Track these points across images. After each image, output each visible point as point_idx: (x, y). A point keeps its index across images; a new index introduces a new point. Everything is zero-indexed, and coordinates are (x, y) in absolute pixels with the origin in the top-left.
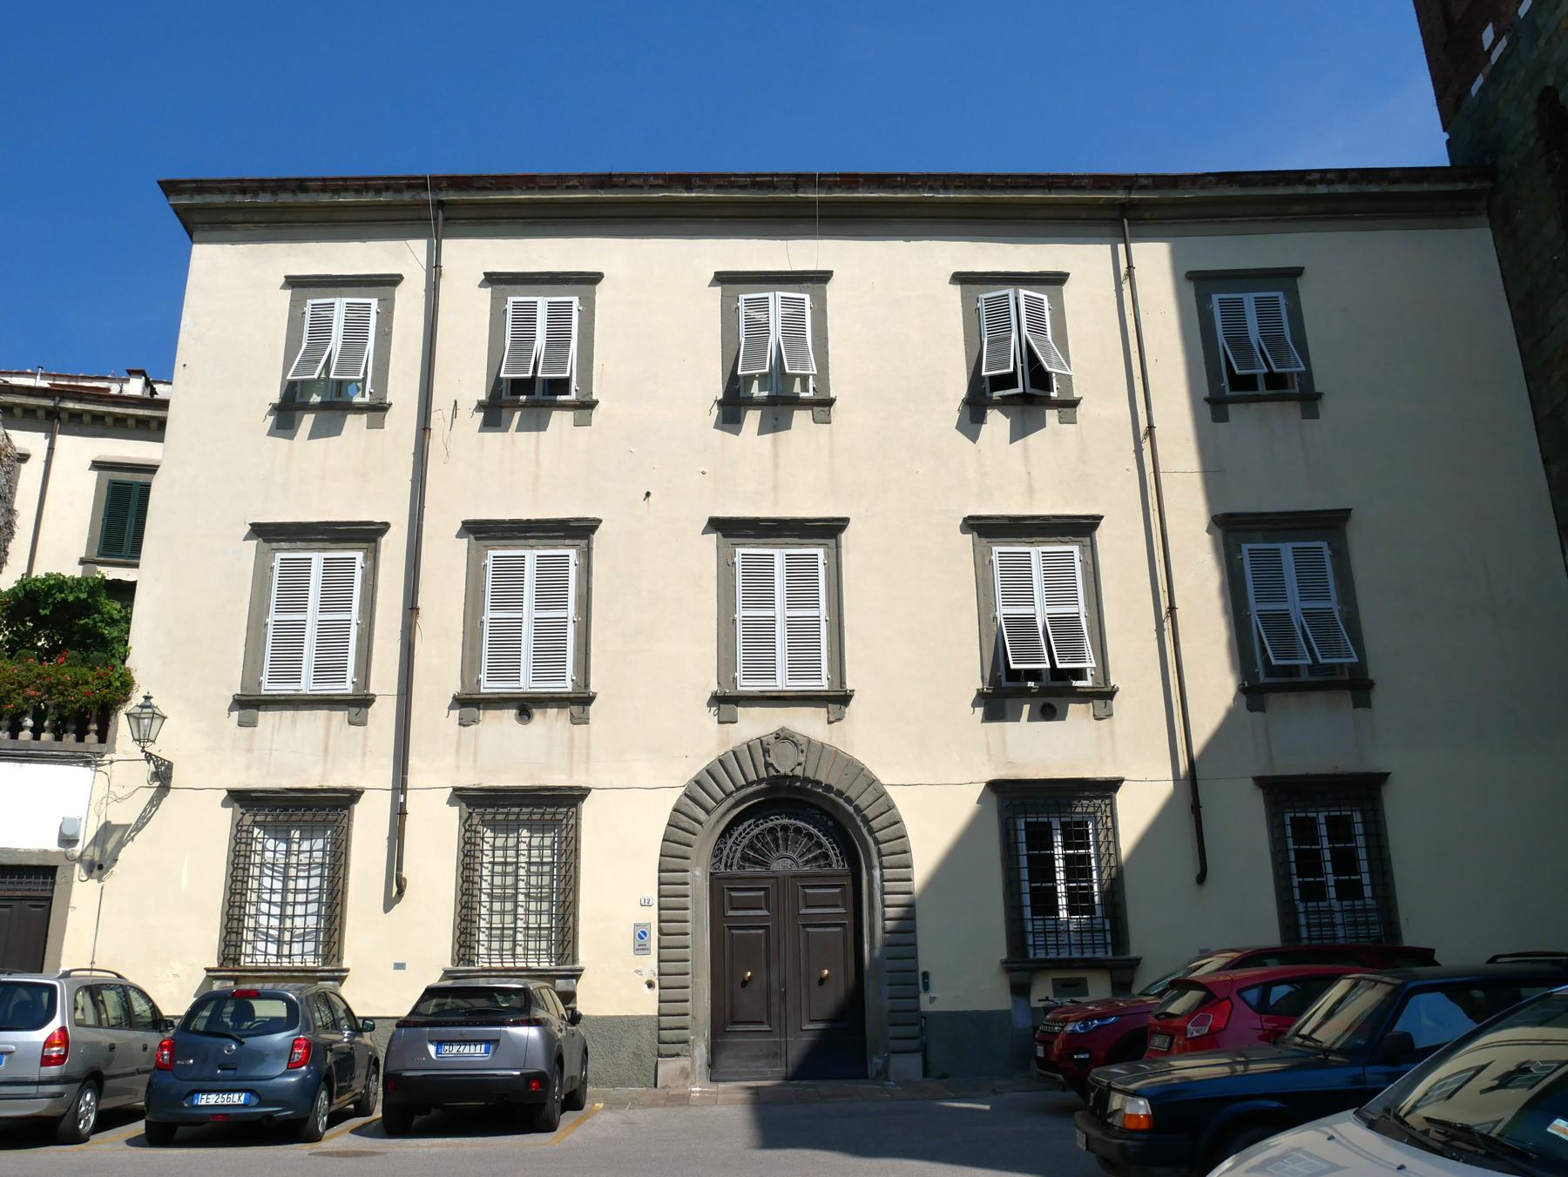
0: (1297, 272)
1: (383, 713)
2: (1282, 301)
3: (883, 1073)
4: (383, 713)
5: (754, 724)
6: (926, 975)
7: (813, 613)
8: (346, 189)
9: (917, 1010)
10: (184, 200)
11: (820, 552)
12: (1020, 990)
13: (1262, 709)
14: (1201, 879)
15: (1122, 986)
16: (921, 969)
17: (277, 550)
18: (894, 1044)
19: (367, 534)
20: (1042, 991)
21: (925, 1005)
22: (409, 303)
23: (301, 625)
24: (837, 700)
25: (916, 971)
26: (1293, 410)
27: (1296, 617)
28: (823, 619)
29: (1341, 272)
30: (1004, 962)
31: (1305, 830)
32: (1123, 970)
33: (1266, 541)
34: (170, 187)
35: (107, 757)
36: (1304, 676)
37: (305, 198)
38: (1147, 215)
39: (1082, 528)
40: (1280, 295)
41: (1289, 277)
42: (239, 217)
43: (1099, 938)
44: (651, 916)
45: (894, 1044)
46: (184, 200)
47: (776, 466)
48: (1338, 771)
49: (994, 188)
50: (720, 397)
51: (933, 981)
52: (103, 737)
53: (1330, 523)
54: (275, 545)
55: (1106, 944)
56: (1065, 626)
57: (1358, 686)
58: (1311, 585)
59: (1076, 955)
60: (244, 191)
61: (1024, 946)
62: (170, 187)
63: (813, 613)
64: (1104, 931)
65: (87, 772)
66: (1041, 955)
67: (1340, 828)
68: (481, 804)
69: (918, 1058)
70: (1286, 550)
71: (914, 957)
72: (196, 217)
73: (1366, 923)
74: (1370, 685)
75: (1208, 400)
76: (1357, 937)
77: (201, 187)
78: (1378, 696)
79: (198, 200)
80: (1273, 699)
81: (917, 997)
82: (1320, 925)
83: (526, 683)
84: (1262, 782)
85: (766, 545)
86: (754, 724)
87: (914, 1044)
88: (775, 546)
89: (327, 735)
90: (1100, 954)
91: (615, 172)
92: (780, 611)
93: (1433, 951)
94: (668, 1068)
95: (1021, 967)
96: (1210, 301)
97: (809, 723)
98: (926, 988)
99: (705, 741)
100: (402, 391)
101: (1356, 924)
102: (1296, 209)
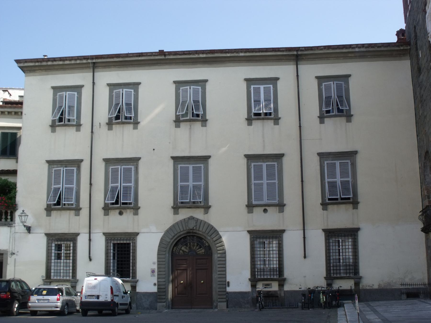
0: (277, 79)
1: (84, 212)
2: (343, 85)
3: (216, 307)
4: (84, 212)
5: (184, 214)
6: (228, 282)
7: (268, 182)
8: (67, 60)
9: (226, 291)
10: (22, 65)
11: (202, 165)
12: (254, 286)
13: (326, 210)
14: (15, 259)
15: (281, 285)
16: (227, 281)
17: (54, 168)
18: (219, 300)
19: (77, 163)
20: (260, 287)
21: (229, 289)
22: (86, 93)
23: (262, 184)
24: (207, 208)
25: (226, 281)
26: (344, 119)
27: (339, 184)
28: (74, 189)
29: (360, 74)
30: (249, 279)
31: (59, 248)
32: (282, 282)
33: (271, 162)
34: (18, 61)
35: (13, 225)
36: (339, 201)
37: (55, 63)
38: (42, 69)
39: (279, 157)
40: (133, 91)
41: (203, 83)
42: (37, 68)
43: (275, 273)
44: (155, 267)
45: (219, 300)
46: (22, 65)
47: (190, 140)
48: (346, 227)
49: (180, 55)
50: (107, 122)
51: (231, 284)
52: (12, 219)
53: (351, 155)
54: (52, 166)
55: (277, 275)
56: (127, 189)
57: (354, 203)
58: (344, 173)
59: (269, 277)
60: (38, 62)
61: (330, 273)
62: (18, 61)
63: (329, 180)
64: (277, 271)
65: (9, 228)
66: (259, 277)
67: (68, 247)
68: (330, 234)
69: (225, 303)
70: (338, 163)
71: (226, 278)
72: (25, 69)
73: (349, 269)
74: (358, 203)
75: (318, 117)
76: (277, 275)
77: (26, 61)
78: (360, 206)
79: (26, 64)
80: (330, 207)
81: (226, 288)
82: (336, 270)
83: (265, 201)
84: (324, 230)
85: (187, 164)
86: (184, 214)
87: (224, 300)
88: (190, 164)
89: (69, 220)
90: (275, 277)
91: (130, 53)
92: (265, 181)
93: (325, 277)
94: (159, 305)
95: (254, 281)
96: (251, 87)
97: (199, 214)
98: (229, 286)
99: (169, 219)
100: (85, 120)
101: (346, 269)
102: (350, 55)
